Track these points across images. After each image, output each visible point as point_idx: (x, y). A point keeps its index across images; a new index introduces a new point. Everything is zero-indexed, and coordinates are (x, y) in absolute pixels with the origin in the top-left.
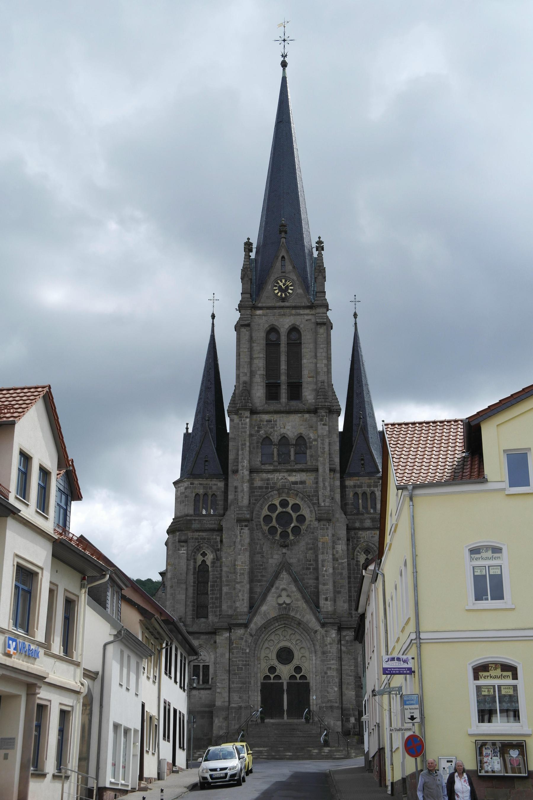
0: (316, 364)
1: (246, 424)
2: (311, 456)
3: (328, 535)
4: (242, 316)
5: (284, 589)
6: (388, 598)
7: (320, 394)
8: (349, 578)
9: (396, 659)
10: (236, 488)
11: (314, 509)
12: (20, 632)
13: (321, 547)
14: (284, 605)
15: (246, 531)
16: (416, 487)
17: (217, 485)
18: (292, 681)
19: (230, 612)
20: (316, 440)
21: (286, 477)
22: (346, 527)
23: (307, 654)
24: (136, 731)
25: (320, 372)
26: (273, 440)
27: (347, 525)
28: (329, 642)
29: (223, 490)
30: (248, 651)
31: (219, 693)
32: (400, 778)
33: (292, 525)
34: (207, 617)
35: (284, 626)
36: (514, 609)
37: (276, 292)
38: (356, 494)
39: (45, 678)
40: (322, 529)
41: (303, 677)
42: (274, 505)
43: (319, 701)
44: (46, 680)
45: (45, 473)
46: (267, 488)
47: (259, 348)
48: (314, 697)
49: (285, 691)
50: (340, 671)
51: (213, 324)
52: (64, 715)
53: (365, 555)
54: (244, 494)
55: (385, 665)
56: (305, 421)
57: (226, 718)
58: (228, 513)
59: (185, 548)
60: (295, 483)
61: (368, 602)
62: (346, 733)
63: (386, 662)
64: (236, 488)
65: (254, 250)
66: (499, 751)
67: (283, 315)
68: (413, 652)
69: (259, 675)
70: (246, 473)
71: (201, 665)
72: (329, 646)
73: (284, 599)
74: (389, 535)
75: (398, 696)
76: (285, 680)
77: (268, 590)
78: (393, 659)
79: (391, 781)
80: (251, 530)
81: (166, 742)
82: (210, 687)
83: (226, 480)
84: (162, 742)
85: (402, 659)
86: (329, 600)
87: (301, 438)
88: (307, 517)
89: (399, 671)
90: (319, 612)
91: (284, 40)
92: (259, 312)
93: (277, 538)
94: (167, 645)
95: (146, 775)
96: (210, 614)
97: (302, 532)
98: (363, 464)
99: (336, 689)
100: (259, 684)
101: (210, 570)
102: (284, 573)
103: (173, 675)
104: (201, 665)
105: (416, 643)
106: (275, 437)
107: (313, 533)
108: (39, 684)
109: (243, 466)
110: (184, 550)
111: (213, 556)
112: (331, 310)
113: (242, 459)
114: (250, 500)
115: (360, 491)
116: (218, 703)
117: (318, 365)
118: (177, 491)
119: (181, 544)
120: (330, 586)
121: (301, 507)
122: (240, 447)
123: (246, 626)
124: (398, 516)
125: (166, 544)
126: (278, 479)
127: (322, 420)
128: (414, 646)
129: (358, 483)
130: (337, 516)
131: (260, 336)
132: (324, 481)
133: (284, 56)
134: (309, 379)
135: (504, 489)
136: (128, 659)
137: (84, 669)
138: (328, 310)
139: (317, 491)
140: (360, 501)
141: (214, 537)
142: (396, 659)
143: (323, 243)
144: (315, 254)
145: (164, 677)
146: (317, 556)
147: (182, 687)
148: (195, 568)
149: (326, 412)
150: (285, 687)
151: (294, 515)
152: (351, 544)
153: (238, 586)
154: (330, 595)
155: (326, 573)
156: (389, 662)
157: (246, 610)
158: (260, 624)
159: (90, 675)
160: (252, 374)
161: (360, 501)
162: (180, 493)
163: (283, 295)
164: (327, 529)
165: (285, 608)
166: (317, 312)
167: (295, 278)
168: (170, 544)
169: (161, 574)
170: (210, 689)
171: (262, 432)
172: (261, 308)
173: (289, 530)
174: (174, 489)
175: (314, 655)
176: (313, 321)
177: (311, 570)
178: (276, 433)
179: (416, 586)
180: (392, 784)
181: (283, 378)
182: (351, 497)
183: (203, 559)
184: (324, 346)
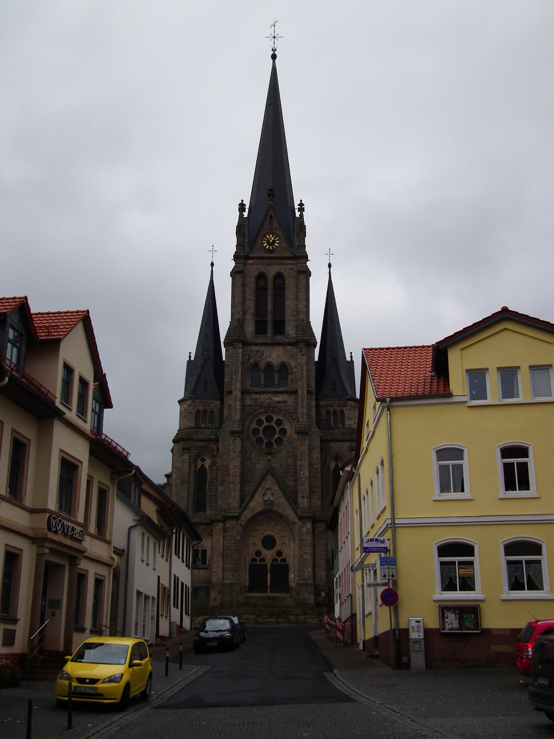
0: (297, 305)
1: (239, 353)
2: (292, 380)
3: (305, 446)
4: (236, 265)
5: (268, 489)
6: (363, 492)
7: (300, 329)
8: (322, 480)
9: (374, 540)
10: (230, 405)
11: (294, 424)
12: (64, 514)
13: (299, 455)
14: (269, 502)
15: (238, 441)
16: (393, 400)
17: (214, 403)
18: (275, 563)
19: (224, 507)
20: (295, 367)
21: (271, 397)
22: (320, 439)
23: (287, 541)
24: (153, 598)
25: (300, 311)
26: (261, 367)
27: (321, 437)
28: (305, 531)
29: (219, 407)
30: (238, 538)
31: (215, 572)
32: (372, 636)
33: (276, 437)
34: (204, 510)
35: (268, 518)
36: (473, 499)
37: (265, 245)
38: (328, 412)
39: (84, 552)
40: (301, 440)
41: (284, 560)
42: (262, 421)
43: (297, 579)
44: (85, 554)
45: (84, 383)
46: (255, 406)
47: (250, 291)
48: (293, 576)
49: (269, 571)
50: (314, 555)
51: (212, 271)
52: (99, 583)
53: (335, 462)
54: (236, 411)
55: (365, 545)
56: (287, 352)
57: (220, 592)
58: (223, 426)
59: (187, 455)
60: (279, 402)
61: (343, 498)
62: (318, 604)
63: (366, 542)
64: (230, 405)
65: (247, 210)
66: (458, 614)
67: (270, 264)
68: (388, 535)
69: (247, 558)
70: (239, 393)
71: (200, 549)
72: (305, 535)
73: (269, 497)
74: (367, 440)
75: (372, 572)
76: (269, 562)
77: (256, 489)
78: (372, 540)
79: (362, 639)
80: (242, 441)
81: (176, 609)
82: (207, 567)
83: (222, 400)
84: (172, 608)
85: (380, 540)
86: (305, 498)
87: (283, 365)
88: (288, 431)
89: (377, 549)
90: (297, 508)
91: (274, 37)
92: (251, 262)
93: (263, 447)
94: (176, 530)
95: (161, 634)
96: (208, 509)
97: (284, 442)
98: (334, 388)
99: (310, 569)
100: (248, 565)
101: (208, 472)
102: (269, 475)
103: (181, 555)
104: (200, 549)
105: (391, 527)
106: (263, 365)
107: (293, 443)
108: (80, 556)
109: (236, 388)
110: (186, 456)
111: (211, 461)
112: (309, 260)
113: (236, 382)
114: (241, 416)
115: (331, 410)
116: (215, 580)
117: (299, 306)
118: (181, 408)
119: (185, 451)
120: (306, 487)
121: (283, 422)
122: (234, 372)
123: (237, 518)
124: (376, 424)
125: (172, 451)
126: (264, 399)
127: (301, 351)
128: (390, 530)
129: (330, 403)
130: (313, 429)
131: (251, 281)
132: (302, 401)
133: (274, 50)
134: (291, 318)
135: (465, 402)
136: (148, 541)
137: (114, 547)
138: (307, 260)
139: (296, 409)
140: (332, 418)
141: (212, 446)
142: (374, 540)
143: (304, 205)
144: (298, 214)
145: (174, 557)
146: (296, 462)
147: (187, 566)
148: (195, 471)
149: (304, 345)
150: (269, 568)
151: (277, 429)
152: (324, 453)
153: (231, 486)
154: (306, 494)
155: (303, 476)
156: (369, 543)
157: (237, 505)
158: (249, 517)
159: (119, 552)
160: (244, 312)
161: (332, 418)
162: (184, 410)
163: (271, 248)
164: (305, 440)
165: (270, 504)
166: (298, 262)
167: (281, 234)
168: (175, 451)
169: (168, 476)
170: (207, 569)
171: (252, 361)
172: (252, 258)
173: (273, 441)
174: (178, 407)
175: (292, 542)
176: (295, 269)
177: (291, 474)
178: (263, 361)
179: (392, 481)
180: (364, 641)
181: (270, 317)
182: (324, 414)
183: (202, 463)
184: (303, 290)
